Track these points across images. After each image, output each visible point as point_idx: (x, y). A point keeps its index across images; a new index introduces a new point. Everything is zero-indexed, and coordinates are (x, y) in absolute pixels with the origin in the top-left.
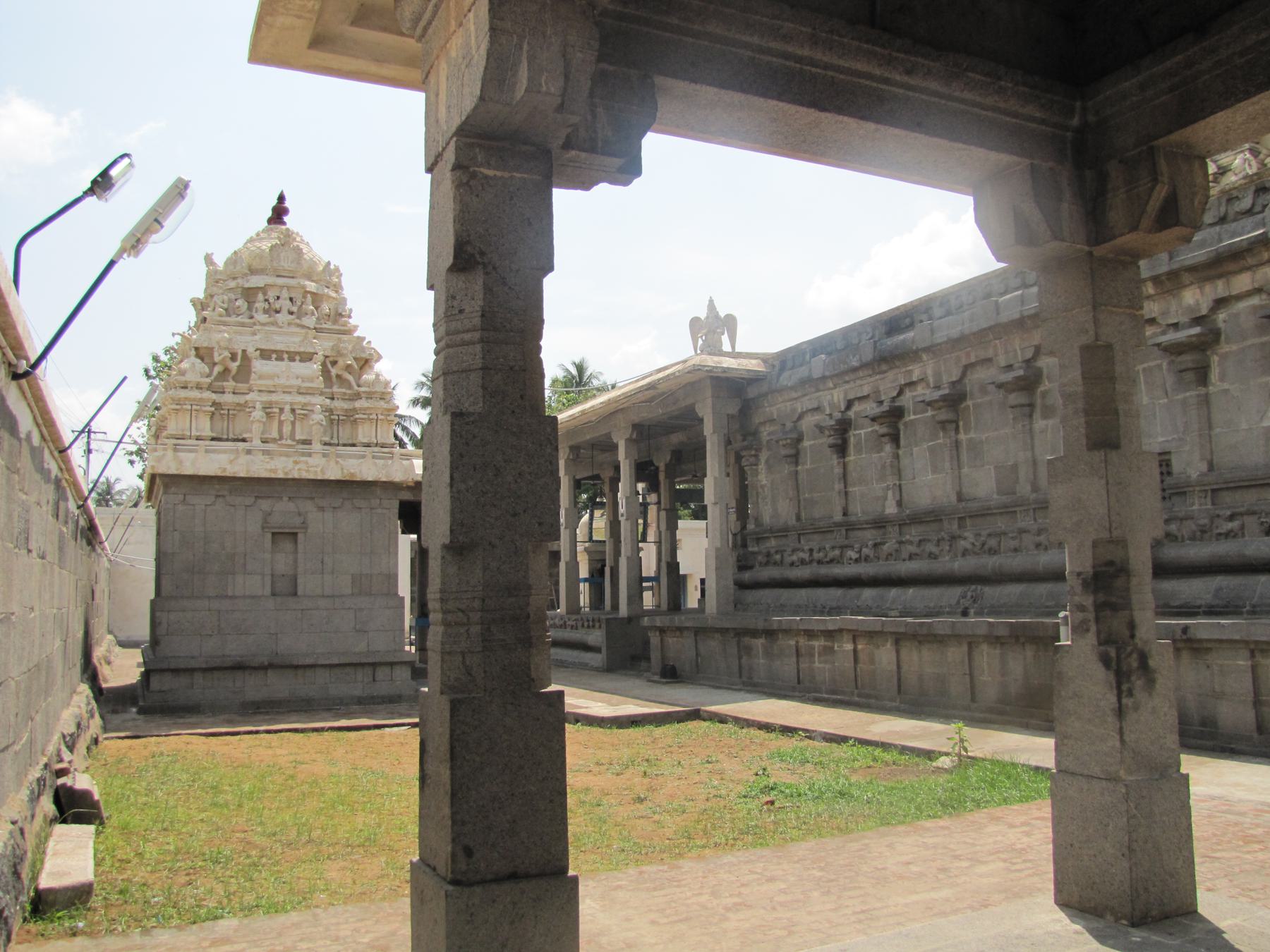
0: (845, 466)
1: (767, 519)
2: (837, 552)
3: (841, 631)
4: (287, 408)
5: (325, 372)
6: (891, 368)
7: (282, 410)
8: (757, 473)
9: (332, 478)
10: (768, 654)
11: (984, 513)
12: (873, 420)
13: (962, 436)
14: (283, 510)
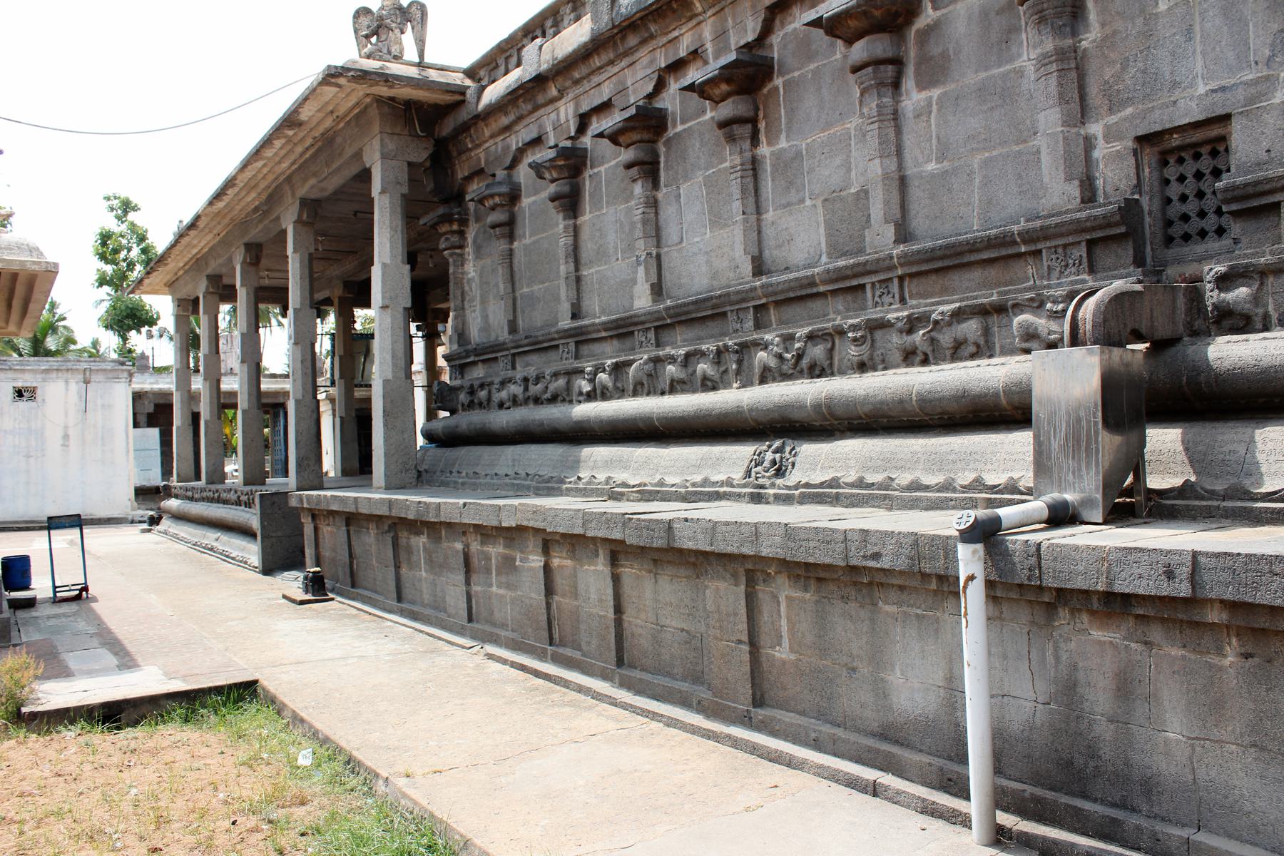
0: (576, 231)
2: (561, 382)
3: (521, 529)
6: (644, 42)
8: (462, 260)
11: (803, 295)
13: (764, 150)
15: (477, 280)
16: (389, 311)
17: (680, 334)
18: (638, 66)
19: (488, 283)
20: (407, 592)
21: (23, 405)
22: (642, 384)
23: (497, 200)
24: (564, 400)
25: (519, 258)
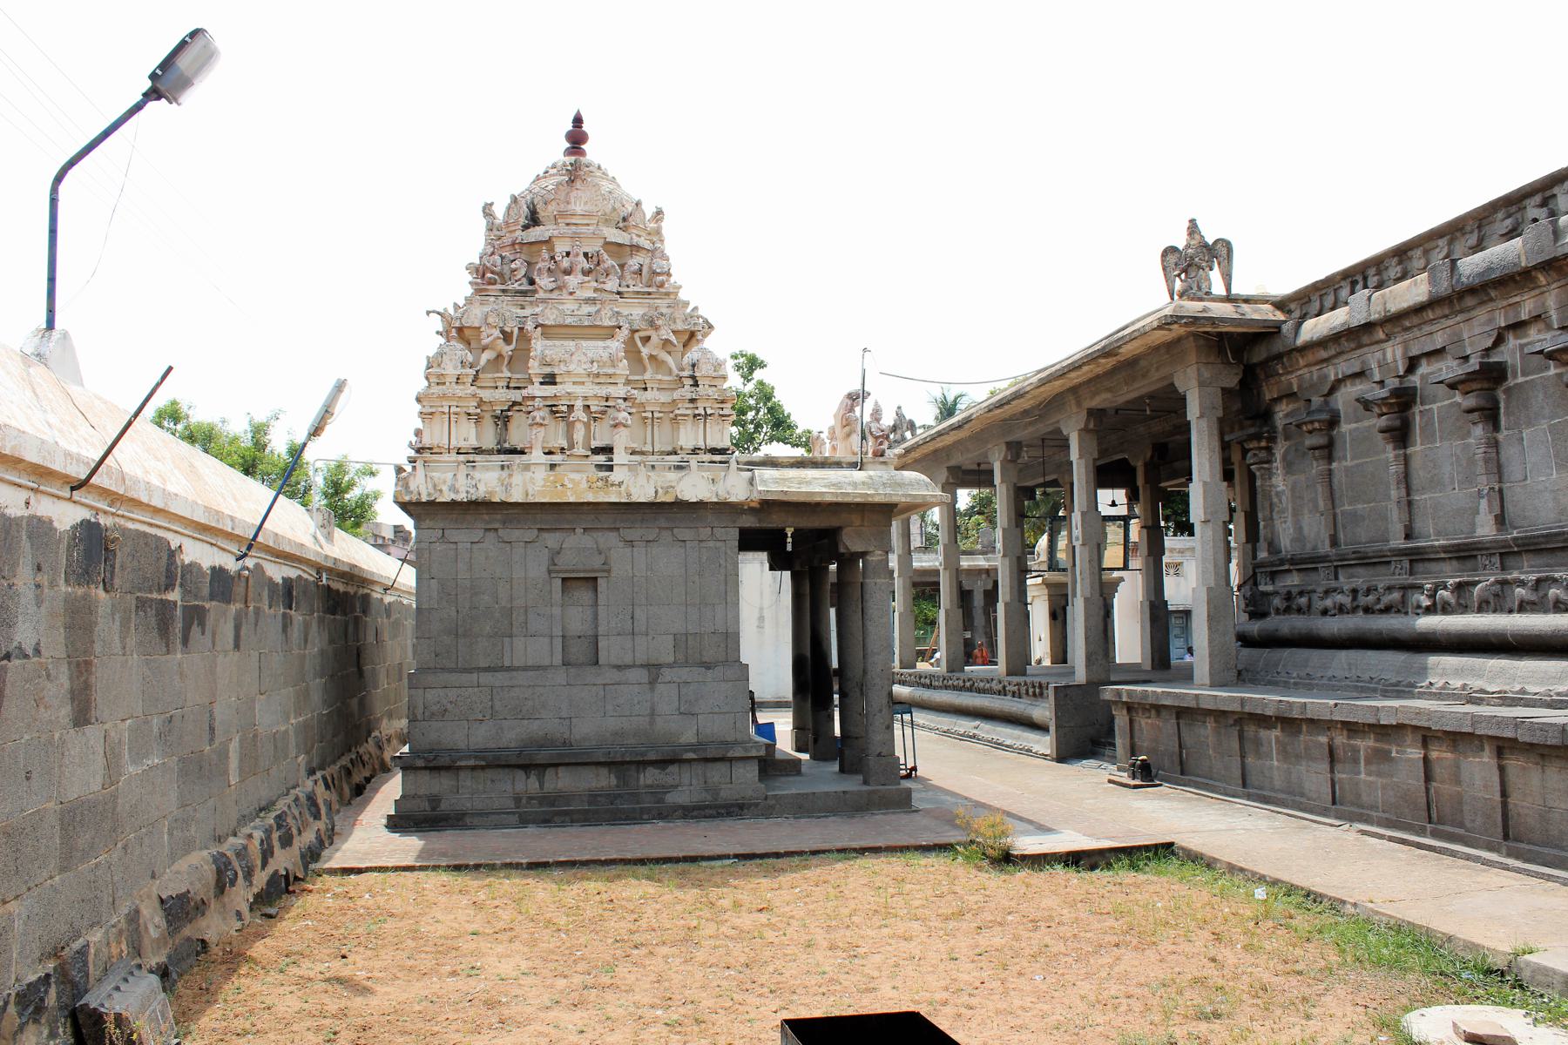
0: (1406, 460)
1: (1286, 543)
2: (1396, 595)
3: (1400, 727)
4: (579, 404)
5: (632, 352)
6: (1482, 303)
7: (571, 407)
8: (1269, 473)
10: (1285, 754)
12: (1452, 386)
14: (577, 547)
15: (1288, 493)
17: (1526, 561)
18: (1475, 322)
19: (1301, 498)
20: (1253, 778)
22: (1488, 602)
23: (1317, 425)
24: (1399, 611)
25: (1339, 478)
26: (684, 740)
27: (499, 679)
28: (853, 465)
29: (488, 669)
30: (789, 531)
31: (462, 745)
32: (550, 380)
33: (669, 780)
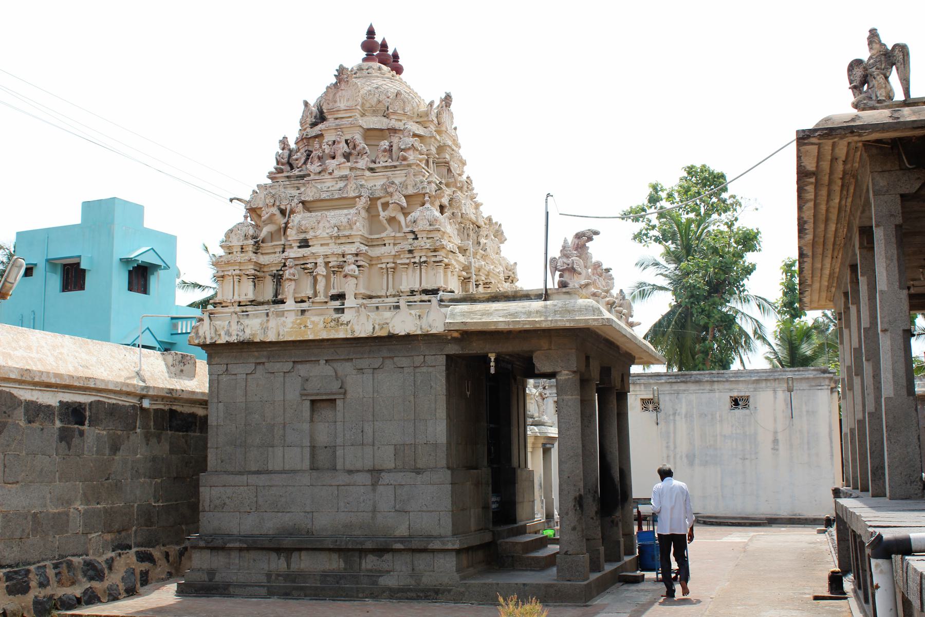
4: (320, 261)
9: (363, 335)
14: (319, 375)
16: (888, 334)
21: (739, 412)
26: (398, 533)
27: (262, 480)
28: (539, 297)
29: (258, 472)
30: (492, 357)
31: (235, 532)
32: (304, 244)
33: (385, 567)
